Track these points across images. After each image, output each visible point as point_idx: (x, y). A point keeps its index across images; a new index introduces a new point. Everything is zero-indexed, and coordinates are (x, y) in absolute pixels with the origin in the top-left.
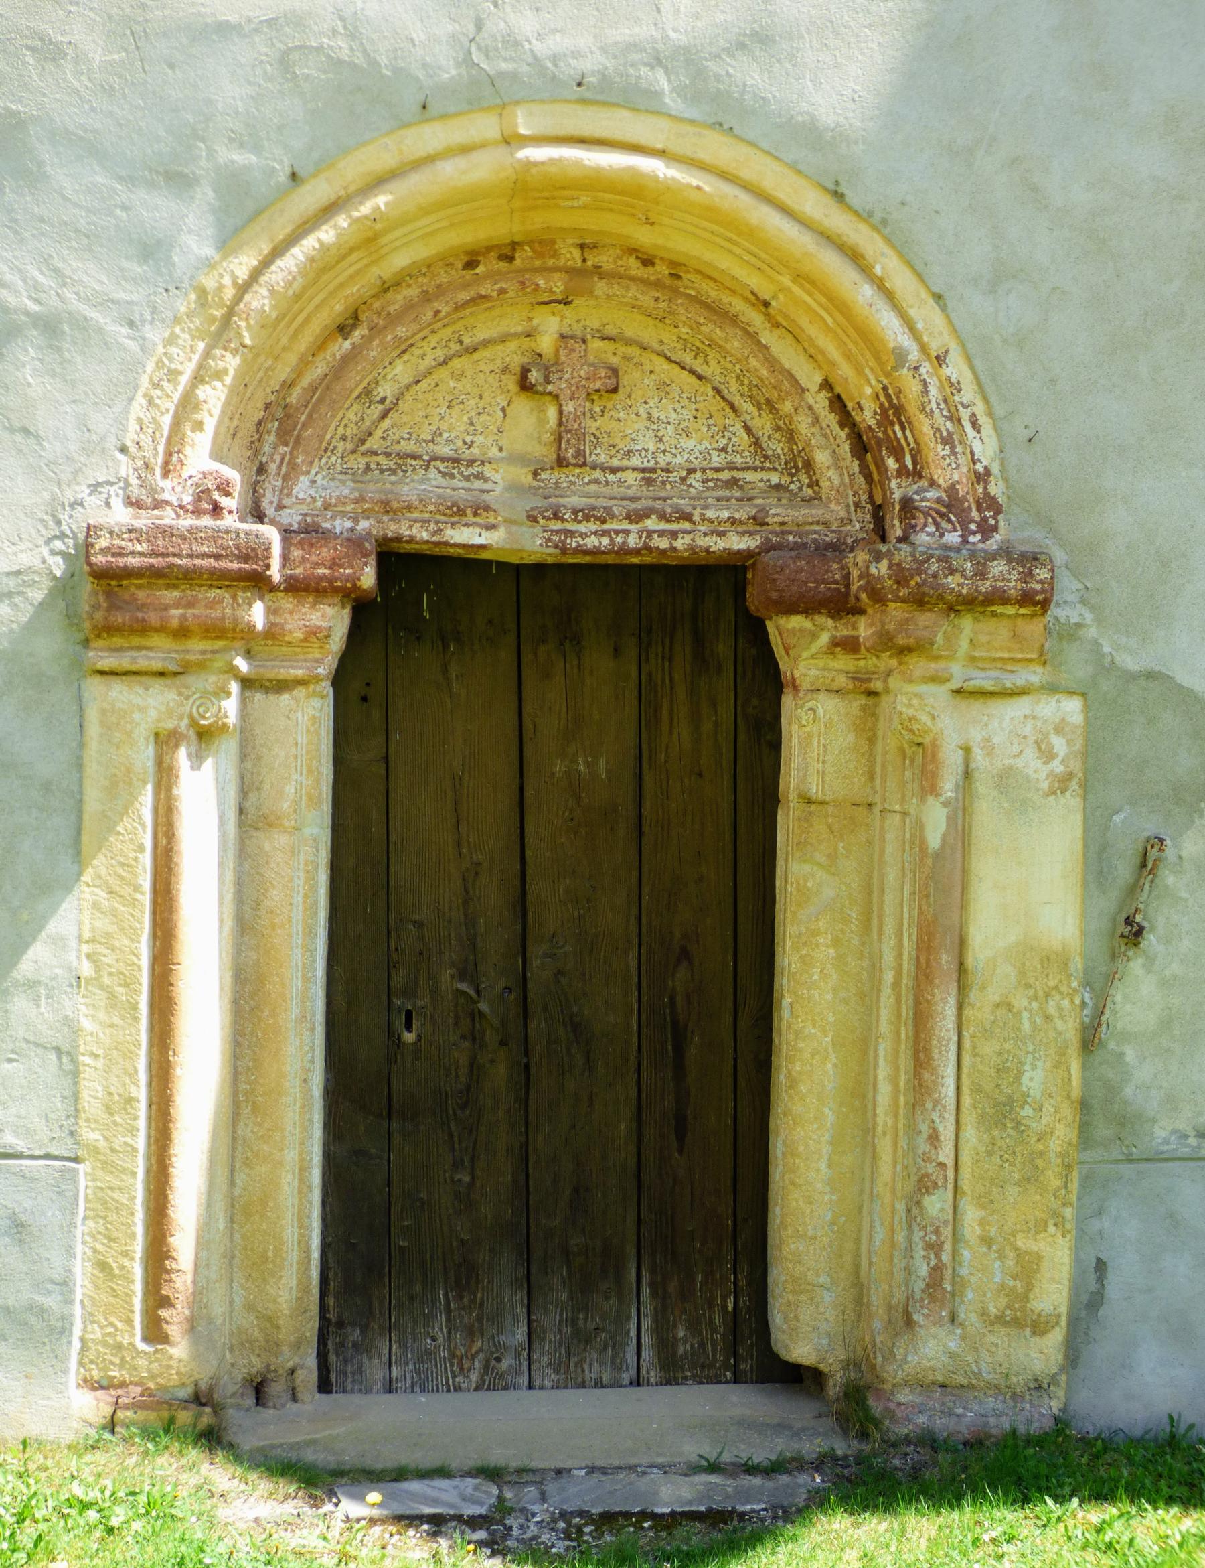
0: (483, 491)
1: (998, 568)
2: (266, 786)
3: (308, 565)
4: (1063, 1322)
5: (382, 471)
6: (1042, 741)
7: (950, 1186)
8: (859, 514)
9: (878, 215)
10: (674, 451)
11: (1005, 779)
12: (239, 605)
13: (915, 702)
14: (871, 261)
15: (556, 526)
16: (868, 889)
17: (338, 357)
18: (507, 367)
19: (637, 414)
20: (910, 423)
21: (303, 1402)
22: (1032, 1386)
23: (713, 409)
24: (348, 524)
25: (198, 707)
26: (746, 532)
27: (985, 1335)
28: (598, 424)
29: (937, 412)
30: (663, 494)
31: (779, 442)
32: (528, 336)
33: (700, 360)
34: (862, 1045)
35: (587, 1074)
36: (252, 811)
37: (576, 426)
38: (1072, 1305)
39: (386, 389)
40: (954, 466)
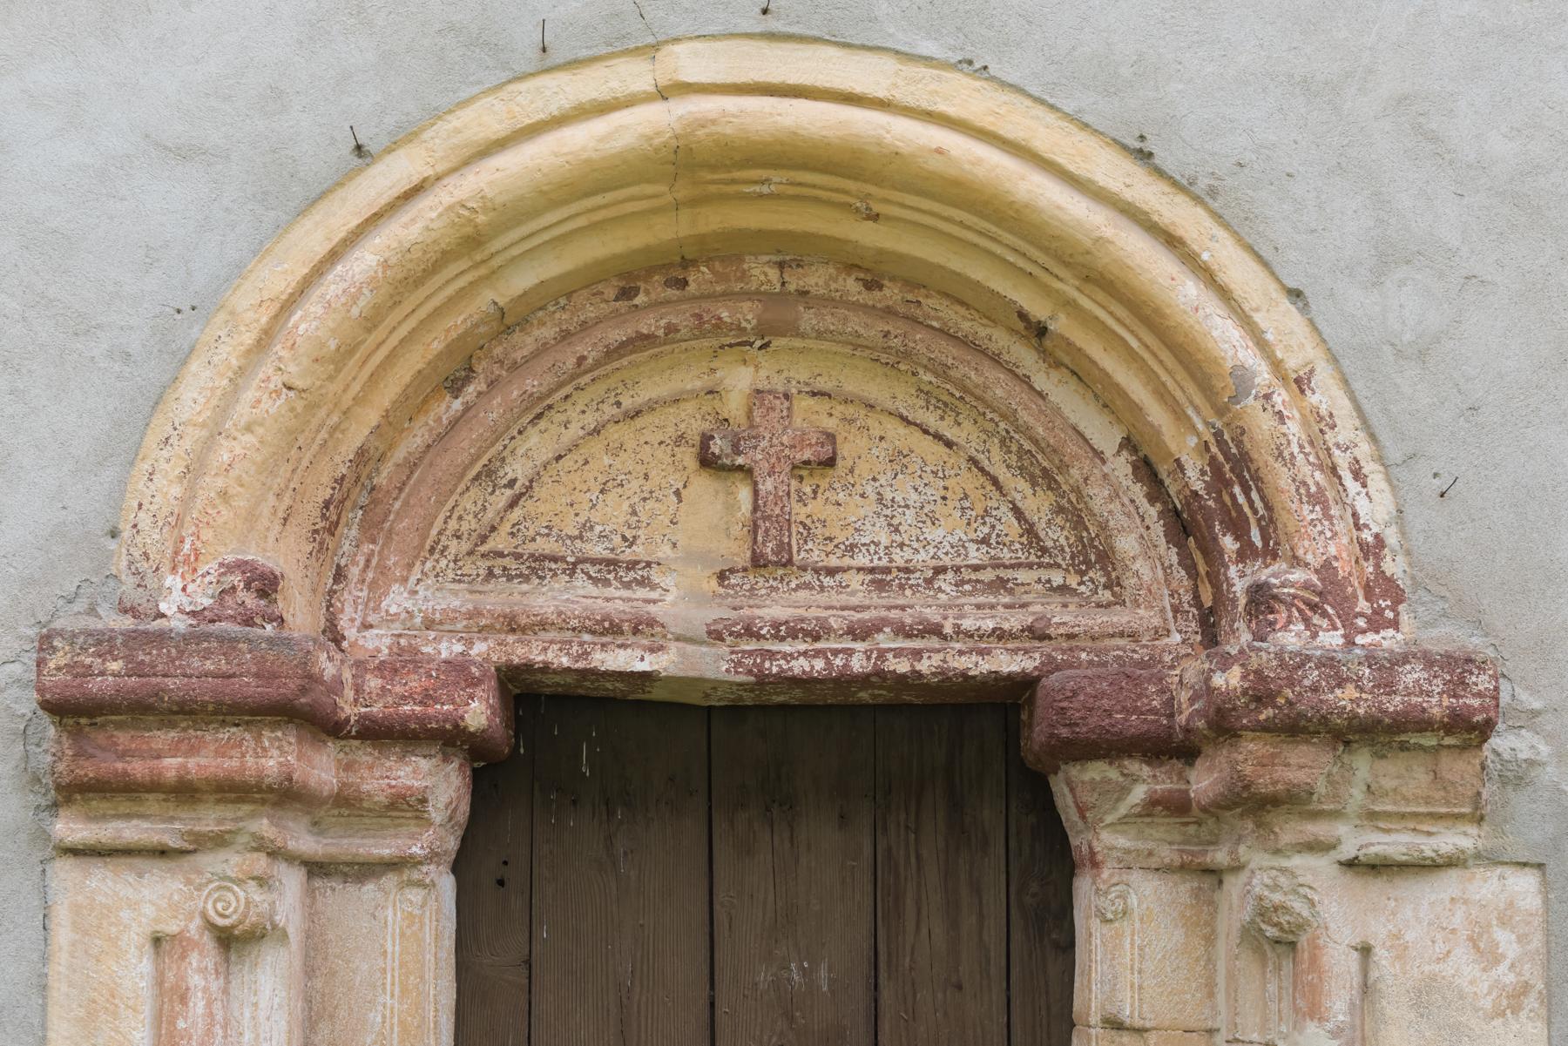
1: (1412, 675)
2: (342, 1013)
5: (510, 578)
6: (1480, 935)
8: (1180, 621)
9: (1203, 183)
10: (915, 545)
11: (1425, 995)
12: (264, 749)
13: (1282, 880)
14: (1196, 248)
15: (752, 645)
17: (445, 422)
18: (682, 436)
19: (862, 496)
23: (969, 487)
25: (215, 902)
30: (901, 601)
31: (1062, 528)
32: (711, 392)
33: (949, 420)
37: (777, 511)
40: (1329, 534)
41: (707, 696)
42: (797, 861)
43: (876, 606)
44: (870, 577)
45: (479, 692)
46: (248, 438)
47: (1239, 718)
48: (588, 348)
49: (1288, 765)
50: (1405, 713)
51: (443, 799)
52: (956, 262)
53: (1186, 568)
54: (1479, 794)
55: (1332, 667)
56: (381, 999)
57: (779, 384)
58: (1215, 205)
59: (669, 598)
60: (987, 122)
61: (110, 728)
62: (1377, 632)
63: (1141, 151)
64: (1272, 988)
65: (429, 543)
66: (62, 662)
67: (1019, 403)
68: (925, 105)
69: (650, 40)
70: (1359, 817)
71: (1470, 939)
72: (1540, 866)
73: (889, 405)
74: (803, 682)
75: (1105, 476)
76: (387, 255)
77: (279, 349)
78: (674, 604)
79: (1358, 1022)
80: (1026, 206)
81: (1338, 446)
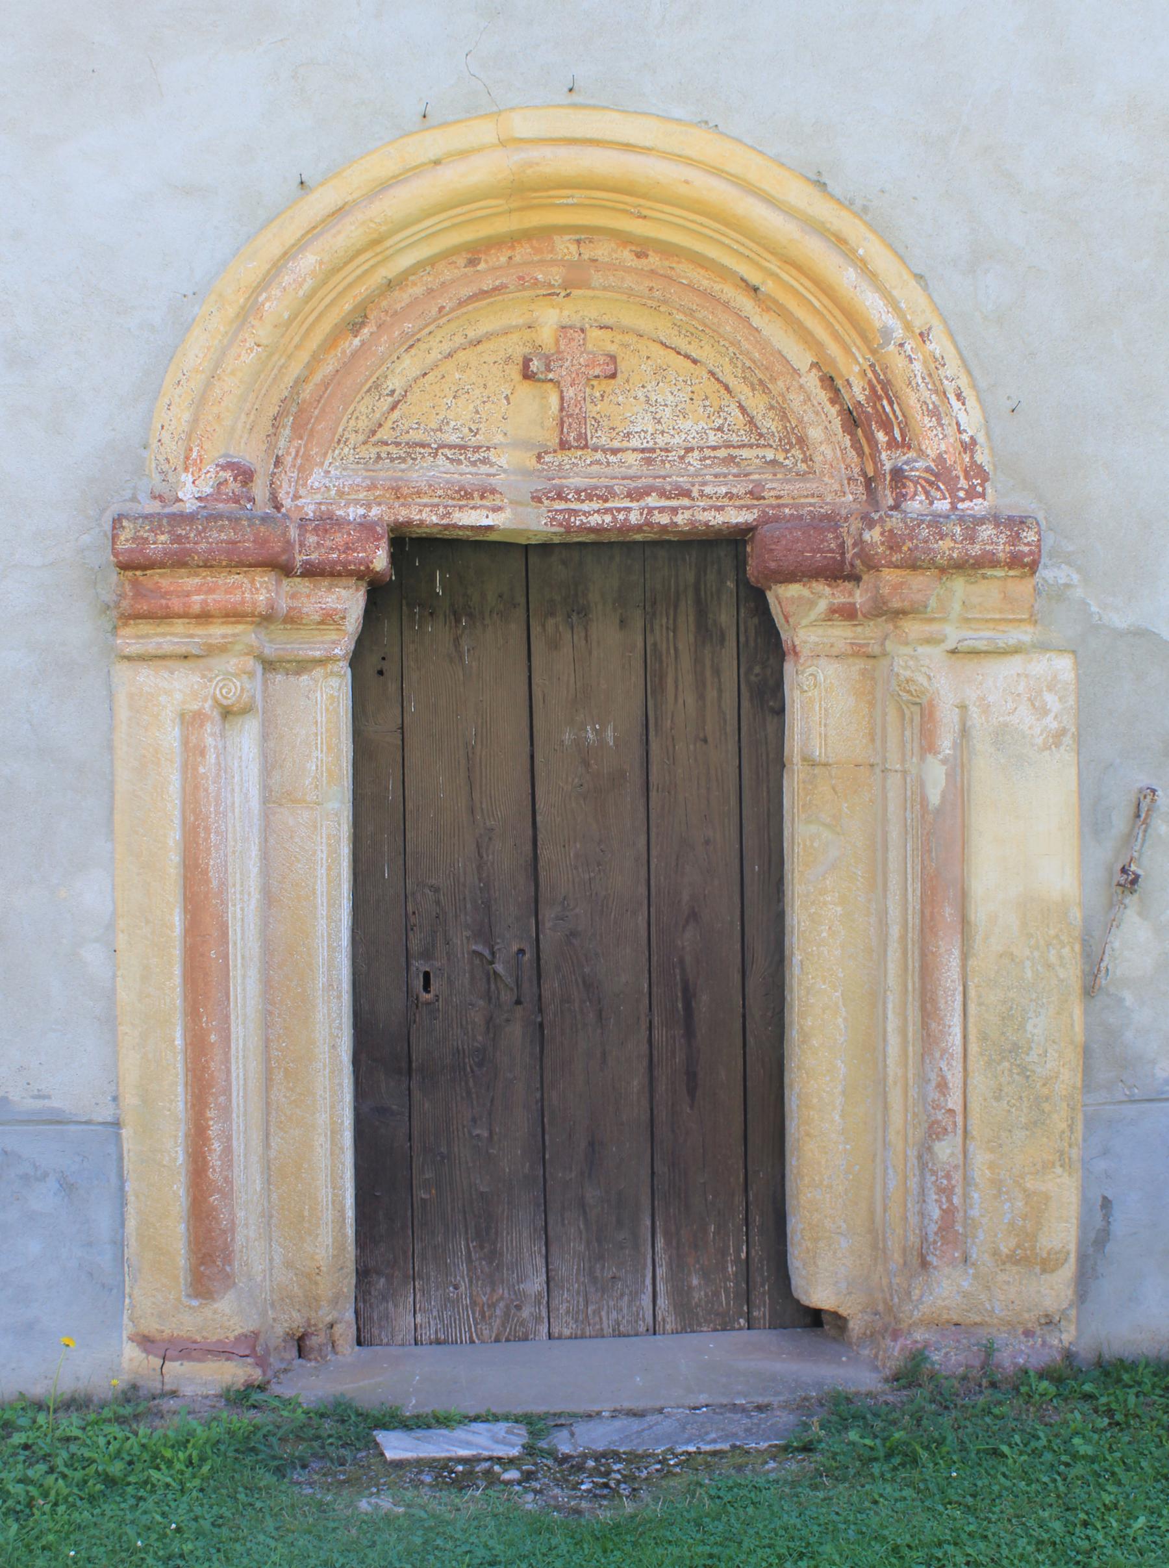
0: (488, 475)
1: (986, 532)
6: (1036, 698)
7: (960, 1132)
10: (672, 432)
11: (1002, 735)
12: (257, 589)
13: (911, 663)
15: (561, 505)
19: (635, 398)
20: (897, 397)
22: (1043, 1321)
24: (361, 511)
25: (221, 689)
35: (599, 1031)
37: (577, 411)
38: (1081, 1243)
39: (395, 383)
40: (941, 436)
41: (529, 539)
42: (590, 653)
53: (856, 449)
55: (937, 527)
56: (315, 754)
57: (576, 320)
58: (868, 218)
65: (337, 437)
69: (495, 109)
71: (1029, 699)
75: (801, 387)
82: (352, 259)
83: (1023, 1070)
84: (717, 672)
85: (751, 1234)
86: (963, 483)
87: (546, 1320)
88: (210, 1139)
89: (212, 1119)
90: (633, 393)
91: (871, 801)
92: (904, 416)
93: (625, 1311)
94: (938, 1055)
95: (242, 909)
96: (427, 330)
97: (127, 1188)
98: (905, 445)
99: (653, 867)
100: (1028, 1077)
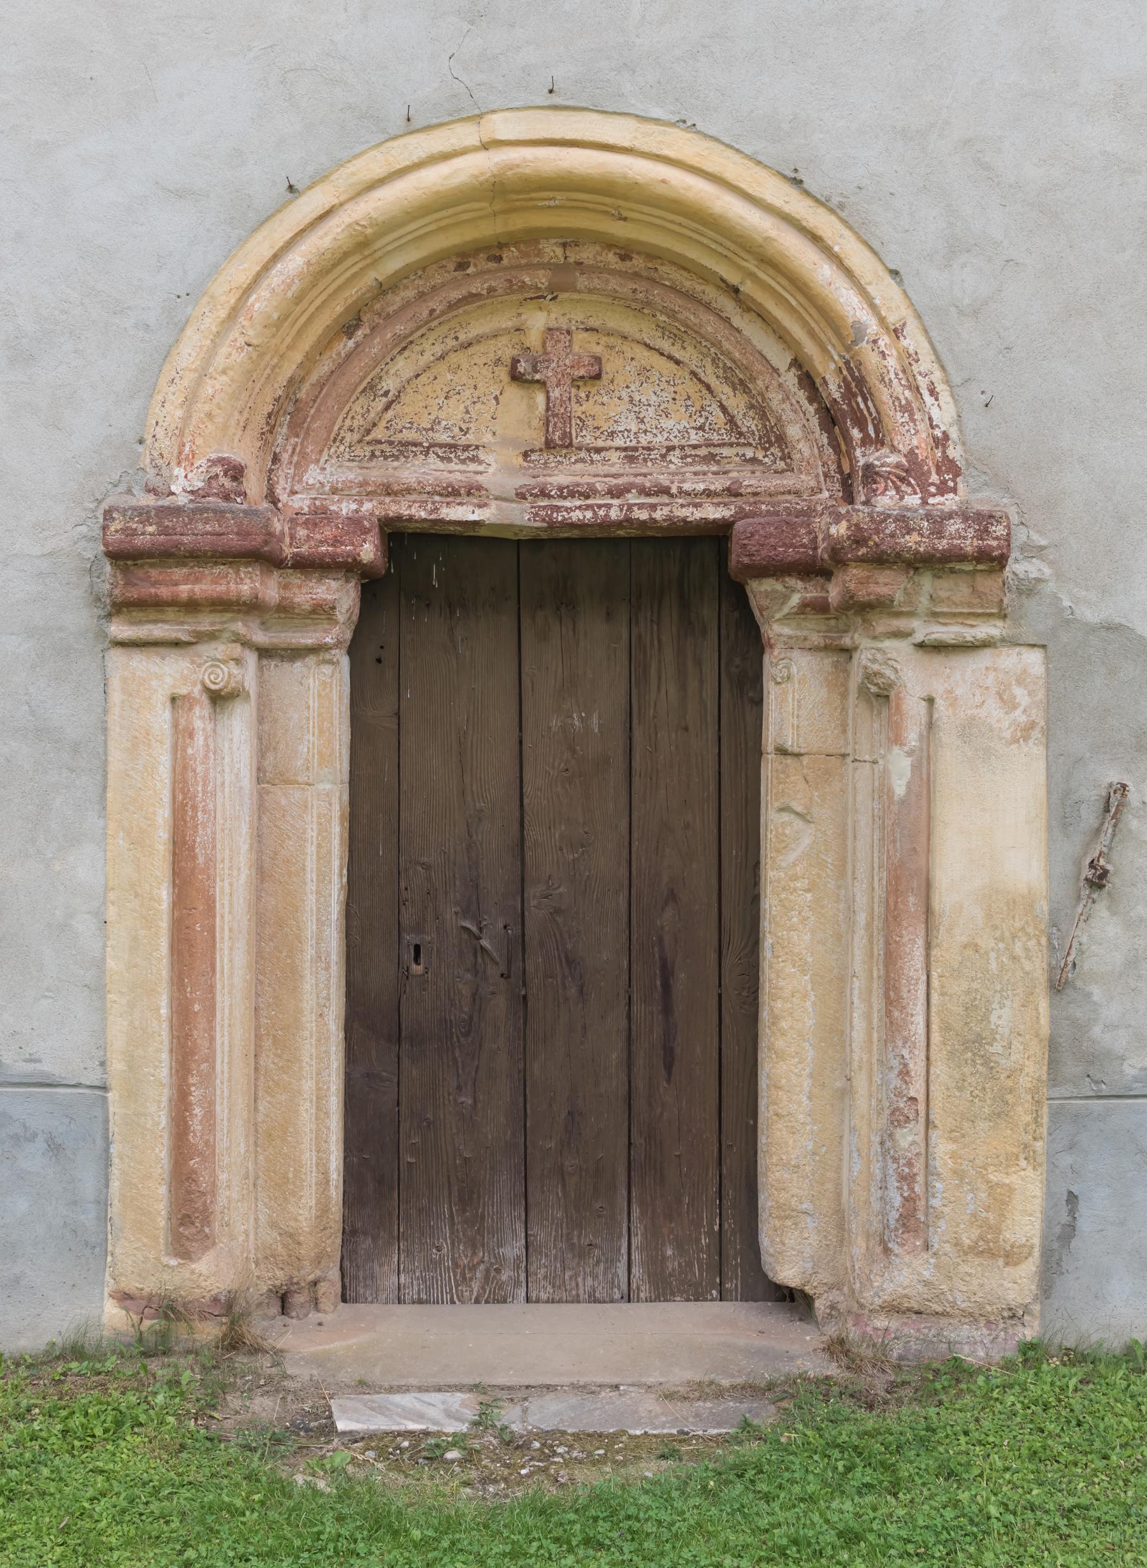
0: (477, 473)
1: (954, 526)
2: (281, 746)
3: (313, 543)
4: (1037, 1253)
5: (386, 458)
6: (1004, 691)
7: (922, 1120)
9: (835, 200)
10: (655, 431)
11: (968, 729)
12: (241, 579)
13: (879, 656)
14: (830, 243)
15: (544, 502)
16: (843, 834)
17: (343, 355)
18: (499, 360)
20: (871, 394)
21: (325, 1312)
22: (1006, 1314)
23: (691, 392)
24: (354, 506)
26: (721, 503)
27: (959, 1264)
28: (583, 408)
29: (895, 381)
30: (644, 470)
32: (518, 330)
33: (678, 345)
34: (836, 984)
35: (580, 1006)
36: (269, 768)
37: (562, 410)
38: (1044, 1237)
39: (390, 384)
41: (516, 534)
43: (627, 474)
44: (624, 454)
45: (369, 538)
46: (224, 379)
47: (846, 554)
48: (436, 304)
49: (877, 583)
50: (949, 550)
51: (345, 607)
52: (679, 247)
54: (1002, 601)
55: (904, 521)
56: (306, 737)
57: (563, 323)
58: (843, 215)
59: (491, 470)
60: (695, 161)
61: (146, 567)
62: (943, 495)
63: (795, 179)
64: (876, 725)
66: (119, 527)
67: (723, 337)
68: (655, 151)
69: (477, 112)
70: (927, 615)
72: (1044, 647)
73: (638, 336)
74: (580, 526)
75: (780, 385)
76: (309, 257)
77: (242, 320)
78: (494, 474)
79: (925, 747)
80: (720, 216)
81: (920, 374)
82: (339, 262)
83: (987, 1061)
84: (698, 663)
85: (724, 1207)
86: (934, 478)
87: (524, 1285)
88: (191, 1104)
89: (194, 1085)
90: (617, 394)
91: (841, 790)
92: (878, 413)
93: (601, 1278)
94: (900, 1043)
95: (231, 885)
96: (419, 333)
97: (112, 1150)
98: (880, 442)
99: (634, 849)
100: (992, 1068)
